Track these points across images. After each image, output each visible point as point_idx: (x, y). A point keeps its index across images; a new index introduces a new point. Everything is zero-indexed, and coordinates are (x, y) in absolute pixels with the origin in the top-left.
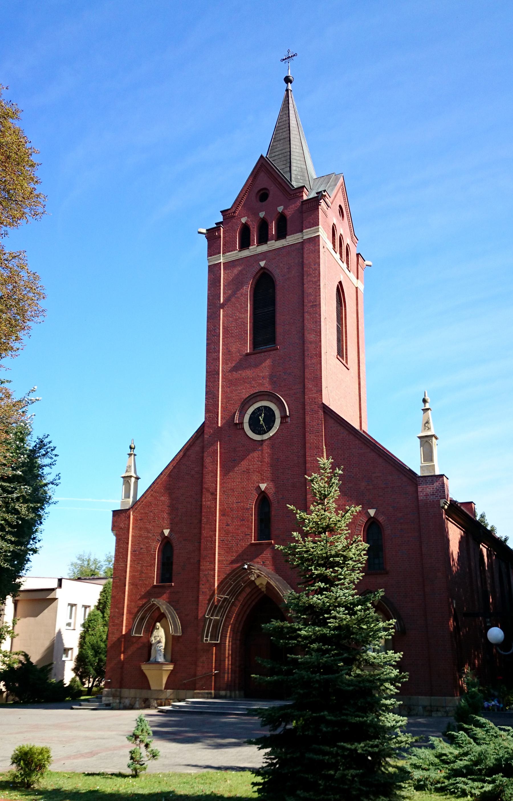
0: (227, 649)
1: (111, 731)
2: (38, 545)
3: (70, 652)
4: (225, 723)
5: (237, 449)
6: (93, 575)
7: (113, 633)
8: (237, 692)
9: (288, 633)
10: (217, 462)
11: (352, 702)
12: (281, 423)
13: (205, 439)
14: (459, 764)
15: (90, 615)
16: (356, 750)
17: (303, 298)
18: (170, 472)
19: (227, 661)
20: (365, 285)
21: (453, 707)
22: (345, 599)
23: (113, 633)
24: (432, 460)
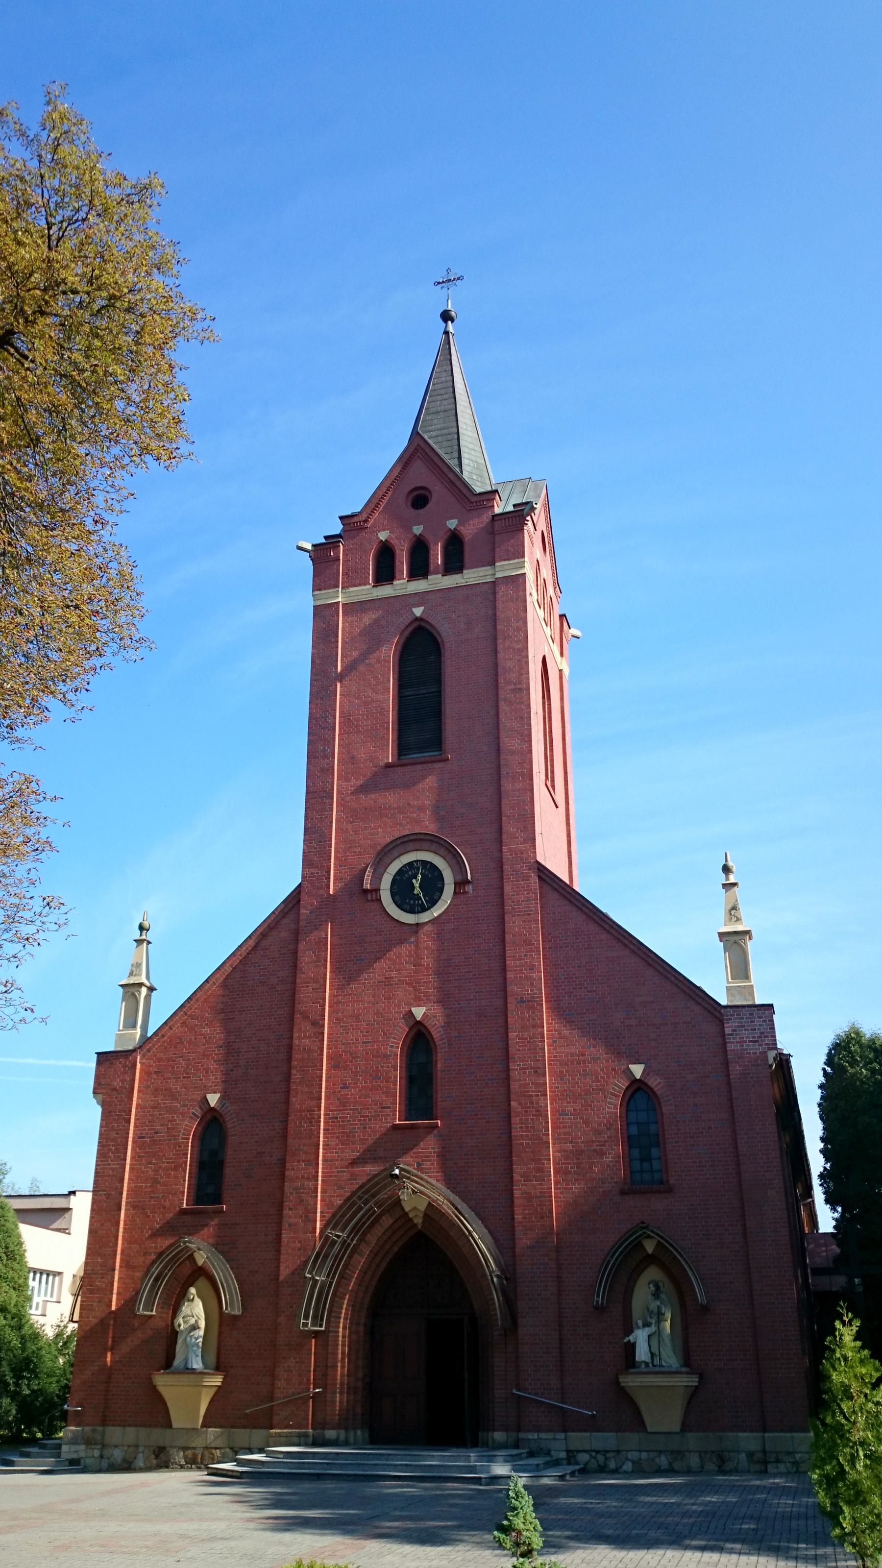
12: (455, 893)
13: (302, 917)
17: (496, 675)
18: (225, 979)
24: (747, 977)
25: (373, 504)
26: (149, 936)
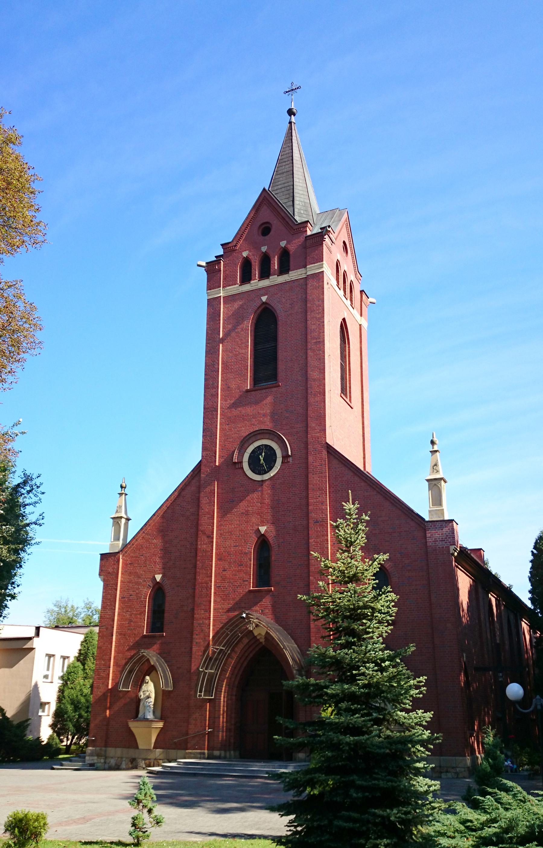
0: (222, 705)
1: (101, 794)
2: (16, 590)
3: (47, 706)
4: (222, 785)
5: (236, 490)
6: (70, 623)
7: (98, 688)
8: (232, 752)
9: (313, 691)
10: (214, 503)
11: (383, 766)
12: (282, 462)
13: (202, 479)
14: (488, 831)
15: (69, 667)
16: (388, 817)
19: (221, 719)
20: (369, 321)
21: (464, 768)
22: (375, 654)
23: (98, 688)
25: (239, 236)
26: (127, 491)
